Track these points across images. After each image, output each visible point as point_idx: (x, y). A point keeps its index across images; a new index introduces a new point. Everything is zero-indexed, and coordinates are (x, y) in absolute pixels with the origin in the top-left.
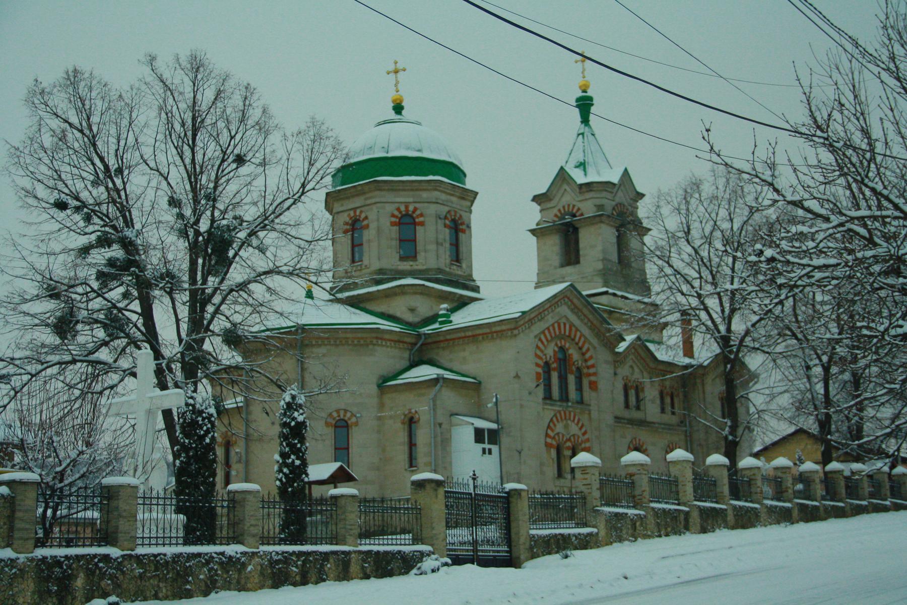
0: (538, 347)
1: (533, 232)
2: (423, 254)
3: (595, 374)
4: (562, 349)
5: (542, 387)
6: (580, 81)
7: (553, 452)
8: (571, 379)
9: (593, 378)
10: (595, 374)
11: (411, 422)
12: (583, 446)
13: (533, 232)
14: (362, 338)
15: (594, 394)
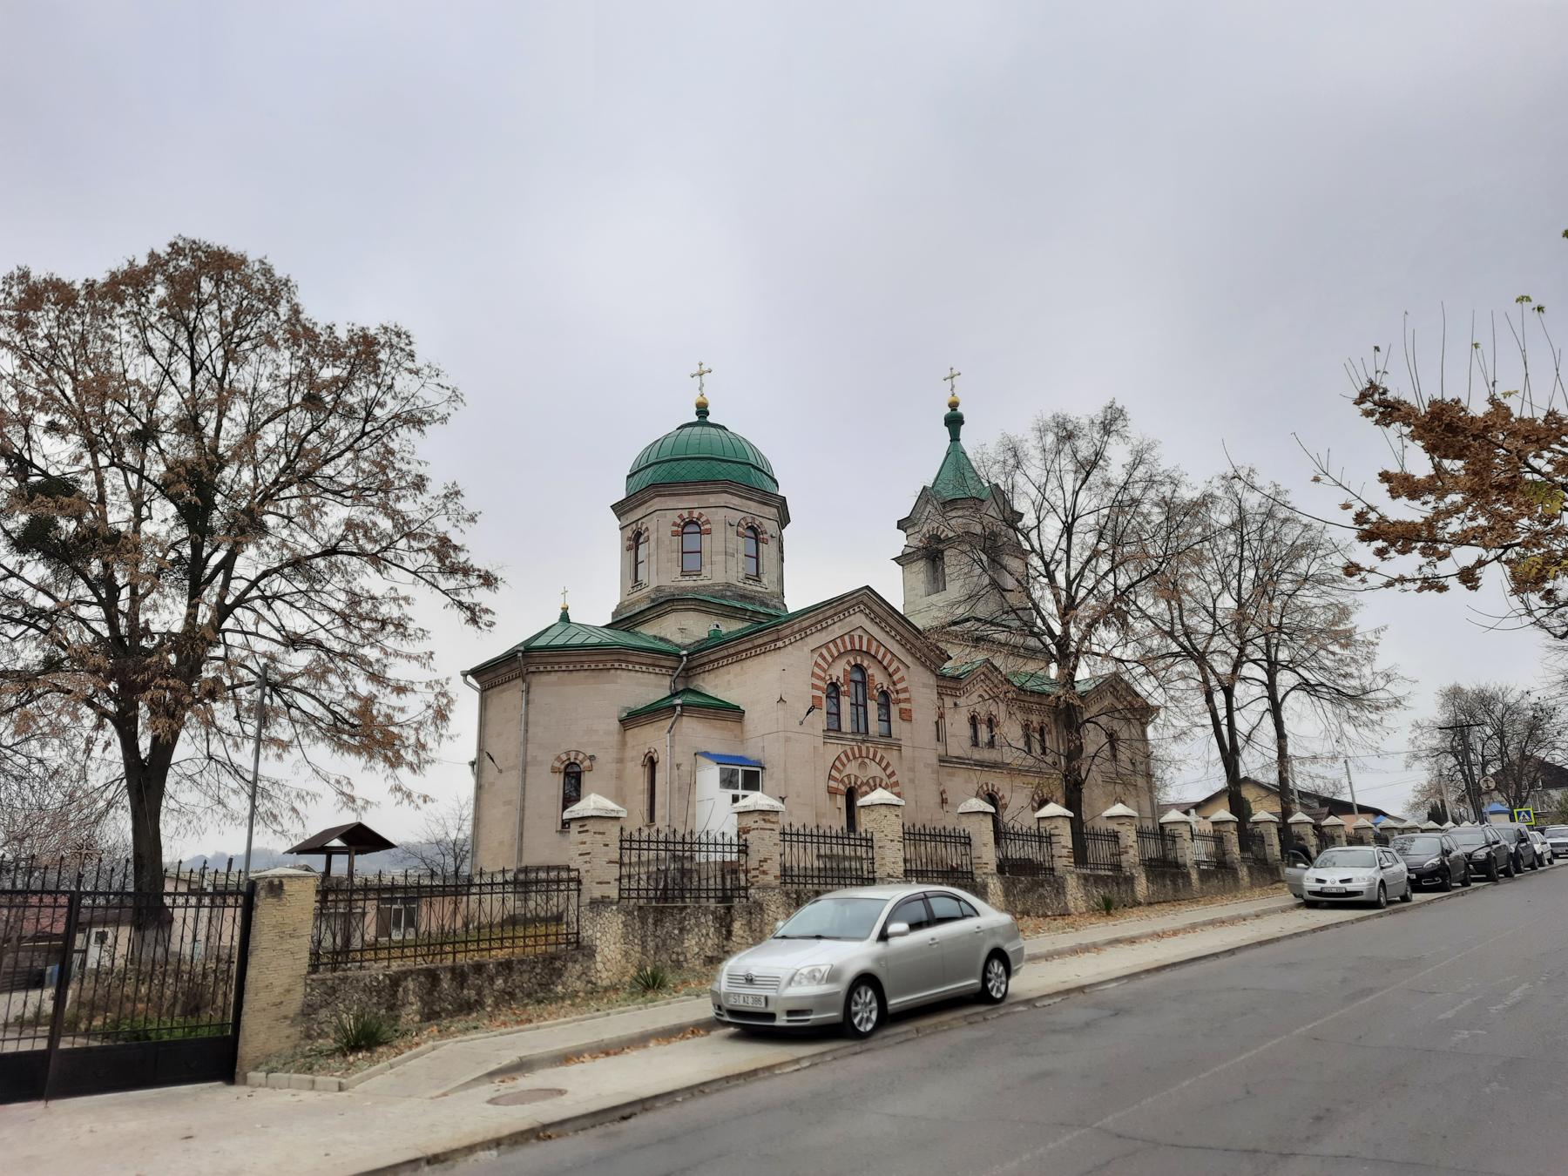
1: (896, 559)
3: (907, 700)
4: (859, 668)
6: (948, 398)
7: (841, 801)
8: (872, 706)
9: (903, 705)
10: (907, 700)
11: (651, 763)
13: (896, 559)
15: (905, 725)
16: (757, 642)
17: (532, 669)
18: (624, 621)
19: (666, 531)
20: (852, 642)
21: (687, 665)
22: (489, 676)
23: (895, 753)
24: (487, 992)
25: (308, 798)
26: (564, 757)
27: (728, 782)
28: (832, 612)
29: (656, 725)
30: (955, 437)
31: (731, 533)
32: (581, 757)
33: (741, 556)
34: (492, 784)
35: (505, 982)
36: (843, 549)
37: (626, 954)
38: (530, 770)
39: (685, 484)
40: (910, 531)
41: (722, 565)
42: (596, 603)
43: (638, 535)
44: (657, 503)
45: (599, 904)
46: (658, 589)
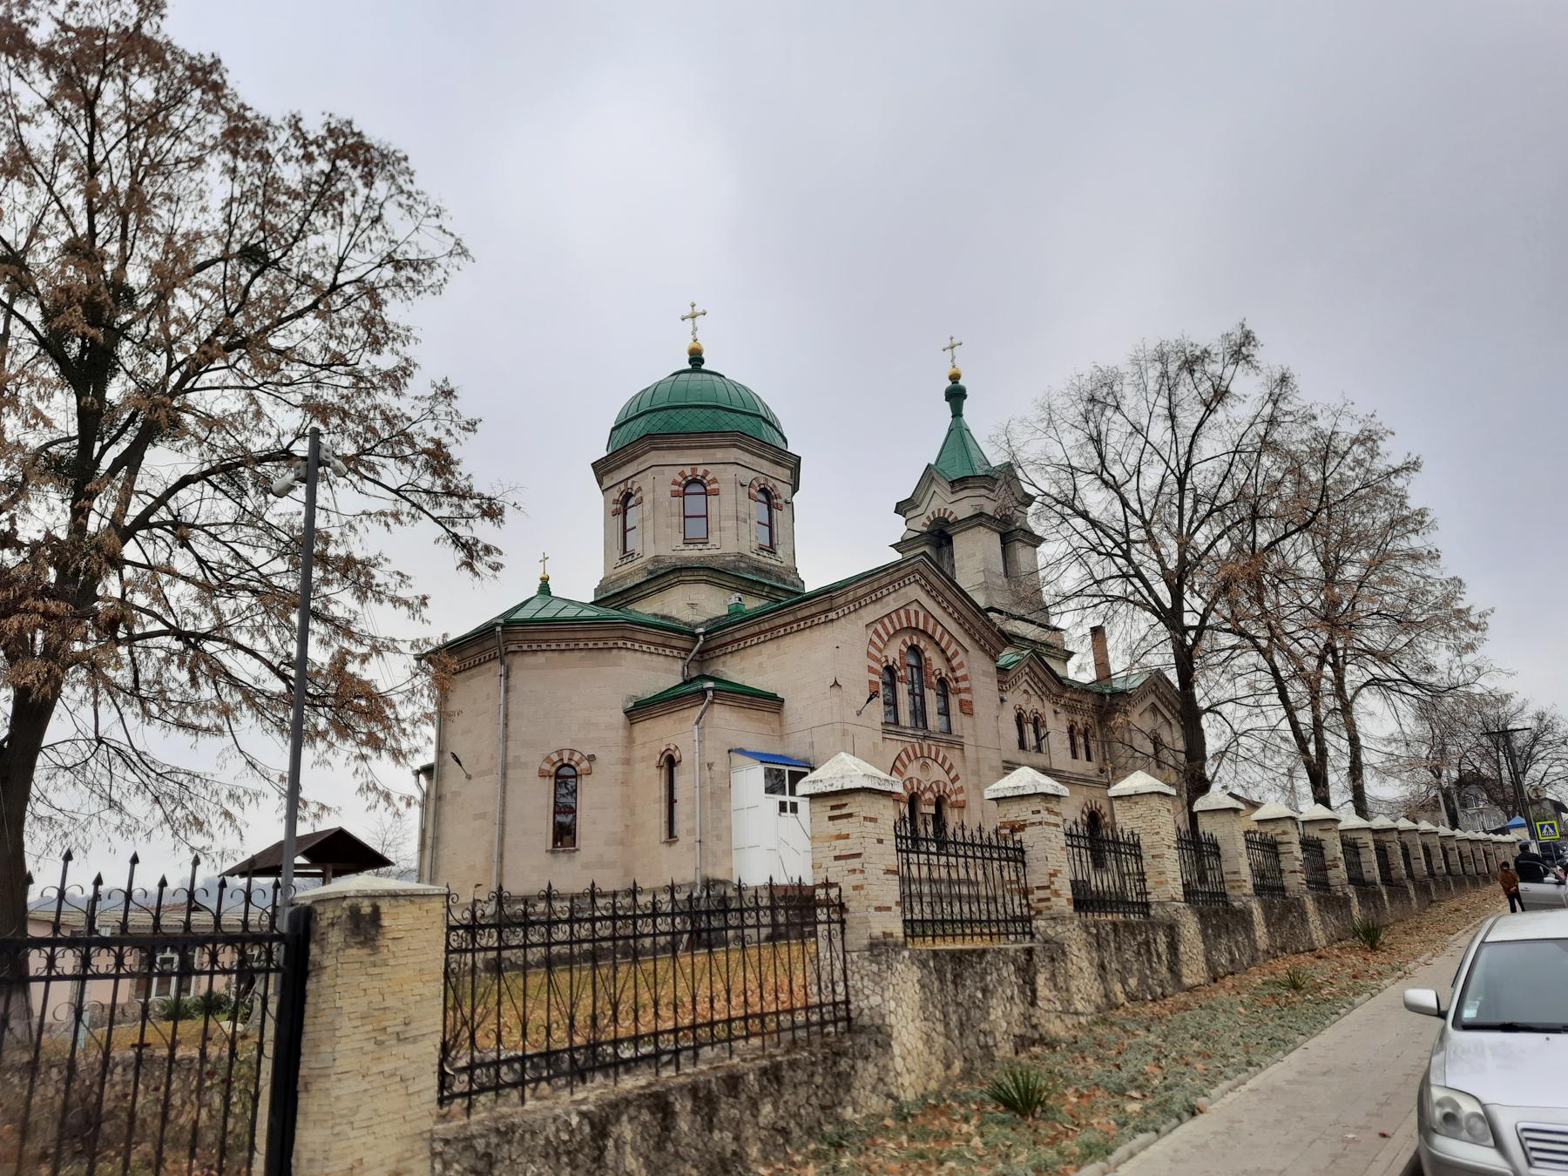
0: (871, 642)
2: (717, 534)
3: (968, 690)
4: (914, 649)
5: (878, 703)
6: (949, 371)
9: (964, 696)
10: (968, 690)
12: (953, 798)
14: (601, 639)
15: (966, 720)
16: (800, 615)
17: (513, 648)
18: (613, 597)
19: (665, 490)
20: (908, 619)
21: (704, 644)
22: (453, 660)
23: (957, 752)
24: (749, 1131)
25: (246, 799)
26: (555, 758)
27: (775, 784)
28: (888, 580)
29: (675, 716)
30: (957, 413)
31: (742, 494)
32: (577, 757)
33: (754, 523)
34: (456, 794)
35: (776, 1108)
36: (841, 531)
37: (928, 1041)
38: (511, 773)
39: (688, 434)
40: (909, 515)
41: (732, 533)
42: (580, 580)
43: (628, 496)
44: (653, 457)
45: (879, 948)
46: (656, 559)
